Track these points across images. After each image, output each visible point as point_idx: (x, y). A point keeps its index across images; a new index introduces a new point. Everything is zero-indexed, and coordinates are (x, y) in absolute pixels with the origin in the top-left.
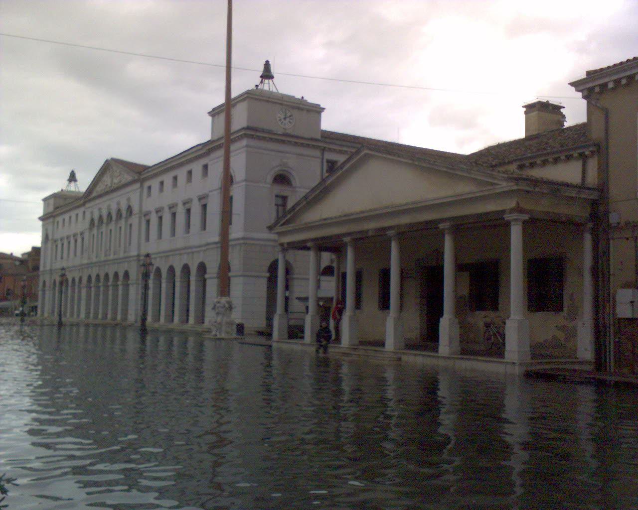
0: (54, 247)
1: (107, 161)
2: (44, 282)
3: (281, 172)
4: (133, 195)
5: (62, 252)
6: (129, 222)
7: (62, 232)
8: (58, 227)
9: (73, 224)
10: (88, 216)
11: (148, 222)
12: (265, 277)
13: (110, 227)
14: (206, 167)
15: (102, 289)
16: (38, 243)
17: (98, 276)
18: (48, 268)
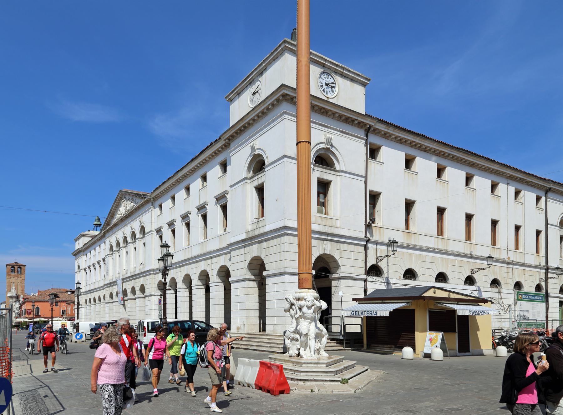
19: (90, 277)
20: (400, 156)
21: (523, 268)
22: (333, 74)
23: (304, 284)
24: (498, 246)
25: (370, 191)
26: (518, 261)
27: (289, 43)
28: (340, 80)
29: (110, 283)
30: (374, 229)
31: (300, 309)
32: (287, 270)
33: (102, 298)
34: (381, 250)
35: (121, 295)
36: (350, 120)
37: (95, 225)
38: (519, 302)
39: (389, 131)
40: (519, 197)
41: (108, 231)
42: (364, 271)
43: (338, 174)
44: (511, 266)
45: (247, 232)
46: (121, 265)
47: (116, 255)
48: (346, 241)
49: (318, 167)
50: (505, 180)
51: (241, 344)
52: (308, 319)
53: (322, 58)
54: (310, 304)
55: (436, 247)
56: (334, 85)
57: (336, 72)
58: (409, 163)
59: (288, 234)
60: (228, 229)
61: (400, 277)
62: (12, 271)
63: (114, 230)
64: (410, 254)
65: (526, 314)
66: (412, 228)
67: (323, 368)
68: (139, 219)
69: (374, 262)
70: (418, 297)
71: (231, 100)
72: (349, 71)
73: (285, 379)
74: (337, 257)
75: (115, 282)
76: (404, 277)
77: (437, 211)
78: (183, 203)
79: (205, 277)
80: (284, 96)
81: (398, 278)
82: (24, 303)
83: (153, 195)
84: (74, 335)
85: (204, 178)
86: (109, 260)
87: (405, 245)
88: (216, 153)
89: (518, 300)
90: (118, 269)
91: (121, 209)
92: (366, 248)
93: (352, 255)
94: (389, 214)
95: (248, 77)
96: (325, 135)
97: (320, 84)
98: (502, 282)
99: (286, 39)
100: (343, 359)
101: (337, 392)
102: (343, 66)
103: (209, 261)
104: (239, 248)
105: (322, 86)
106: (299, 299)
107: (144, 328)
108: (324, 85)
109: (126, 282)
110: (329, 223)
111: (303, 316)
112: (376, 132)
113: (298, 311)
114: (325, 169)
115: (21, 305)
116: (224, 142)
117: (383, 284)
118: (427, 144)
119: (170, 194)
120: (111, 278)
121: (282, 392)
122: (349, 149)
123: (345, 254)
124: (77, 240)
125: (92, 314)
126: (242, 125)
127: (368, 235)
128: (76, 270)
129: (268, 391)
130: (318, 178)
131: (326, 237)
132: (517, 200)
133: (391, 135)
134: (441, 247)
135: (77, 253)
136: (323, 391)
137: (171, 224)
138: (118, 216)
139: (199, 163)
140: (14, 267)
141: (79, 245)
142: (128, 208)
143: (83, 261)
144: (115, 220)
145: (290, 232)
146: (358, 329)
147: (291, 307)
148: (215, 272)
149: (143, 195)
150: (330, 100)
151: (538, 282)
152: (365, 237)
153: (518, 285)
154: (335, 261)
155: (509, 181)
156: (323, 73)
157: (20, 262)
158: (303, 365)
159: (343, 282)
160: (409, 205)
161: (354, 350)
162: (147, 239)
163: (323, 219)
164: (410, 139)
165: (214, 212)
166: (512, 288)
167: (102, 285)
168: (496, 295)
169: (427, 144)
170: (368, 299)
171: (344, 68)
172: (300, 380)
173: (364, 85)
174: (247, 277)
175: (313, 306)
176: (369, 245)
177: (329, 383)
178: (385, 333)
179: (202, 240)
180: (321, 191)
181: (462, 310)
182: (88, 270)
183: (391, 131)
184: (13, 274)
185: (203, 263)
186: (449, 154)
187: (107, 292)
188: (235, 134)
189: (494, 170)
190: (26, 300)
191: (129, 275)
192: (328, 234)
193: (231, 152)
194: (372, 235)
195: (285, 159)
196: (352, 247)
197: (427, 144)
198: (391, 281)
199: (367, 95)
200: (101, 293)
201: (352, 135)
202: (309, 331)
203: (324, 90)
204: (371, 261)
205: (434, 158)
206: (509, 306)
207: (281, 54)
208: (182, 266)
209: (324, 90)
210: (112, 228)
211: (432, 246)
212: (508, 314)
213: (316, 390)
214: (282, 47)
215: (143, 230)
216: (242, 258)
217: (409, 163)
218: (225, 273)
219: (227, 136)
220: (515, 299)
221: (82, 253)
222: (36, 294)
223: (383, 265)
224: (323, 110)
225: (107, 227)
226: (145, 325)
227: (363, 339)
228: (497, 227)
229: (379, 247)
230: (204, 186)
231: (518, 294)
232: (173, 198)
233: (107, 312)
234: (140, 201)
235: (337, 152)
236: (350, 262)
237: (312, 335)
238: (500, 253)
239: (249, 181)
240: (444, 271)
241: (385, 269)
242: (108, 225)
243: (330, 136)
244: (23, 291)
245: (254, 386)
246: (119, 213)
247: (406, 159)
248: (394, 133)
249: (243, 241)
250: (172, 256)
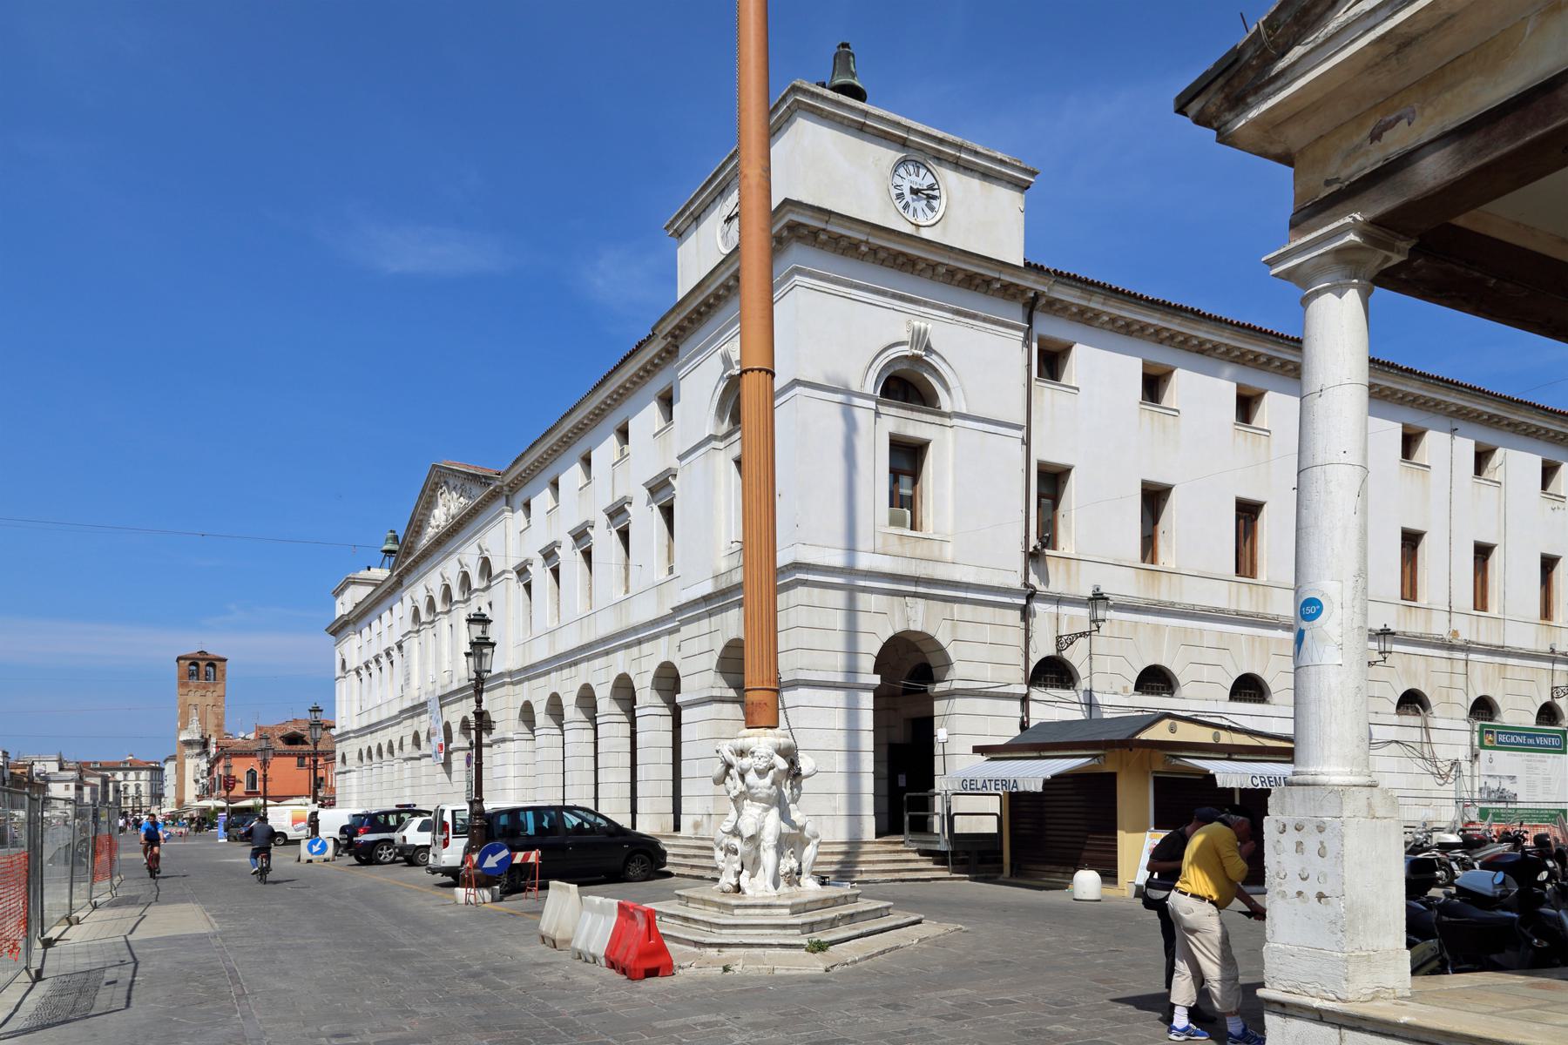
19: (370, 692)
20: (1128, 368)
21: (1498, 660)
22: (932, 164)
23: (756, 717)
24: (1422, 600)
25: (1041, 464)
26: (1482, 640)
27: (806, 92)
28: (950, 179)
29: (414, 708)
30: (1051, 565)
31: (742, 777)
32: (802, 675)
33: (396, 745)
34: (1071, 618)
35: (439, 738)
36: (978, 281)
37: (386, 552)
38: (1484, 754)
39: (1092, 305)
40: (1490, 465)
41: (408, 570)
42: (1022, 674)
43: (947, 421)
44: (1462, 655)
45: (716, 577)
46: (438, 661)
47: (427, 633)
48: (970, 595)
49: (890, 405)
50: (1446, 422)
51: (693, 867)
52: (760, 800)
53: (898, 125)
54: (762, 765)
55: (1233, 607)
56: (936, 193)
57: (940, 158)
58: (1154, 385)
59: (805, 583)
60: (676, 572)
61: (1125, 689)
62: (191, 675)
63: (422, 568)
64: (1157, 627)
65: (1508, 786)
66: (1167, 556)
67: (784, 916)
68: (476, 540)
69: (1049, 650)
70: (1121, 742)
71: (680, 235)
72: (976, 153)
73: (661, 938)
74: (943, 638)
75: (424, 704)
76: (1136, 689)
77: (1237, 510)
78: (576, 497)
79: (624, 691)
80: (793, 227)
81: (1120, 690)
82: (217, 759)
83: (508, 479)
84: (304, 844)
85: (623, 434)
86: (412, 645)
87: (1142, 603)
88: (649, 371)
89: (1482, 746)
90: (431, 670)
91: (436, 512)
92: (1026, 613)
93: (988, 634)
94: (1098, 524)
95: (715, 176)
96: (909, 323)
97: (894, 192)
98: (1433, 700)
99: (797, 83)
100: (857, 896)
101: (784, 972)
102: (959, 140)
103: (635, 651)
104: (698, 618)
105: (900, 196)
106: (742, 753)
107: (445, 826)
108: (907, 192)
109: (448, 704)
110: (922, 549)
111: (746, 795)
112: (1056, 308)
113: (739, 782)
114: (912, 410)
115: (213, 763)
116: (663, 344)
117: (1078, 707)
118: (1202, 335)
119: (547, 475)
120: (416, 694)
121: (652, 973)
122: (980, 357)
123: (966, 631)
124: (338, 592)
125: (375, 787)
126: (700, 299)
127: (1034, 580)
128: (338, 673)
129: (624, 972)
130: (891, 435)
131: (913, 589)
132: (1485, 475)
133: (1097, 315)
134: (1246, 606)
135: (340, 628)
136: (752, 970)
137: (549, 554)
138: (430, 533)
139: (610, 396)
140: (196, 665)
141: (345, 605)
142: (453, 511)
143: (354, 649)
144: (424, 542)
145: (811, 577)
146: (989, 826)
147: (727, 773)
148: (648, 679)
149: (486, 477)
150: (925, 234)
151: (1547, 699)
152: (1026, 585)
153: (1483, 708)
154: (941, 650)
155: (1457, 424)
156: (903, 162)
157: (213, 652)
158: (737, 911)
159: (959, 704)
160: (1154, 498)
161: (976, 880)
162: (498, 589)
163: (906, 541)
164: (1154, 322)
165: (645, 518)
166: (1465, 714)
167: (395, 712)
168: (1416, 735)
169: (1202, 332)
170: (1032, 744)
171: (960, 147)
172: (711, 945)
173: (1022, 187)
174: (716, 693)
175: (772, 768)
176: (1037, 606)
177: (778, 951)
178: (1050, 833)
179: (621, 596)
180: (906, 466)
181: (1231, 775)
182: (364, 672)
183: (1096, 303)
184: (194, 682)
185: (620, 654)
186: (1270, 360)
187: (405, 730)
188: (686, 323)
189: (1406, 395)
190: (225, 753)
191: (455, 686)
192: (917, 581)
193: (679, 369)
194: (1045, 578)
195: (798, 390)
196: (987, 613)
197: (1202, 332)
198: (1099, 698)
199: (1027, 211)
200: (393, 734)
201: (985, 320)
202: (762, 828)
203: (906, 206)
204: (1043, 648)
205: (1229, 369)
206: (1455, 763)
207: (787, 120)
208: (575, 663)
209: (906, 206)
210: (416, 563)
211: (1222, 604)
212: (1453, 787)
213: (737, 969)
214: (789, 102)
215: (486, 565)
216: (704, 644)
217: (1154, 385)
218: (668, 680)
219: (668, 327)
220: (1472, 745)
221: (350, 627)
222: (252, 736)
223: (1075, 656)
224: (901, 260)
225: (407, 558)
226: (448, 818)
227: (1001, 853)
228: (1420, 548)
229: (1065, 610)
230: (624, 456)
231: (1483, 732)
232: (555, 485)
233: (408, 782)
234: (480, 493)
235: (944, 366)
236: (982, 652)
237: (769, 839)
238: (1428, 621)
239: (721, 445)
240: (1257, 671)
241: (1082, 670)
242: (409, 554)
243: (923, 325)
244: (219, 726)
245: (603, 961)
246: (433, 522)
247: (1144, 375)
248: (1105, 309)
249: (706, 599)
250: (493, 645)
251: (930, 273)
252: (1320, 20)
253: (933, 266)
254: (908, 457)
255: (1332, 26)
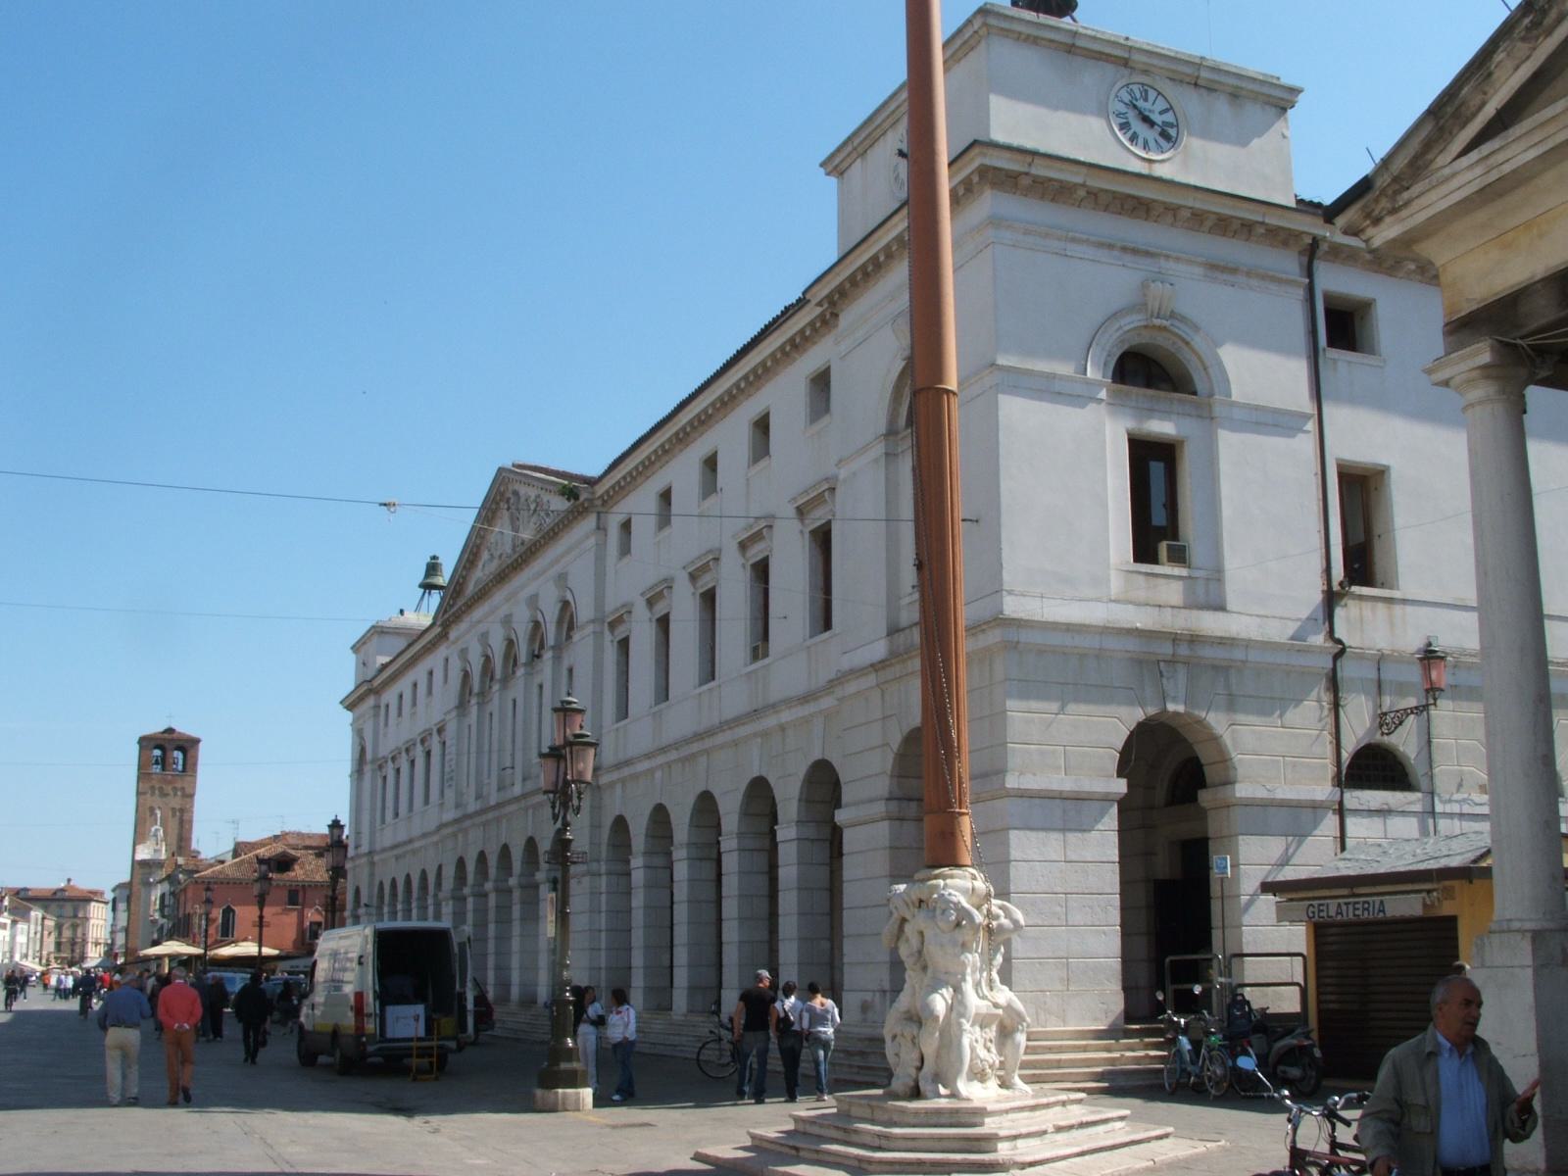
0: (380, 781)
1: (501, 470)
2: (357, 891)
3: (1145, 338)
4: (575, 556)
5: (469, 762)
6: (566, 664)
7: (398, 733)
8: (386, 724)
9: (420, 707)
10: (456, 667)
11: (624, 645)
12: (1106, 798)
13: (511, 694)
14: (821, 382)
15: (492, 900)
16: (1234, 398)
17: (482, 857)
18: (365, 849)
80: (984, 172)
167: (432, 827)
219: (824, 291)
223: (1405, 742)
251: (1169, 219)
252: (952, 746)
253: (1173, 210)
254: (1153, 465)
255: (954, 736)
